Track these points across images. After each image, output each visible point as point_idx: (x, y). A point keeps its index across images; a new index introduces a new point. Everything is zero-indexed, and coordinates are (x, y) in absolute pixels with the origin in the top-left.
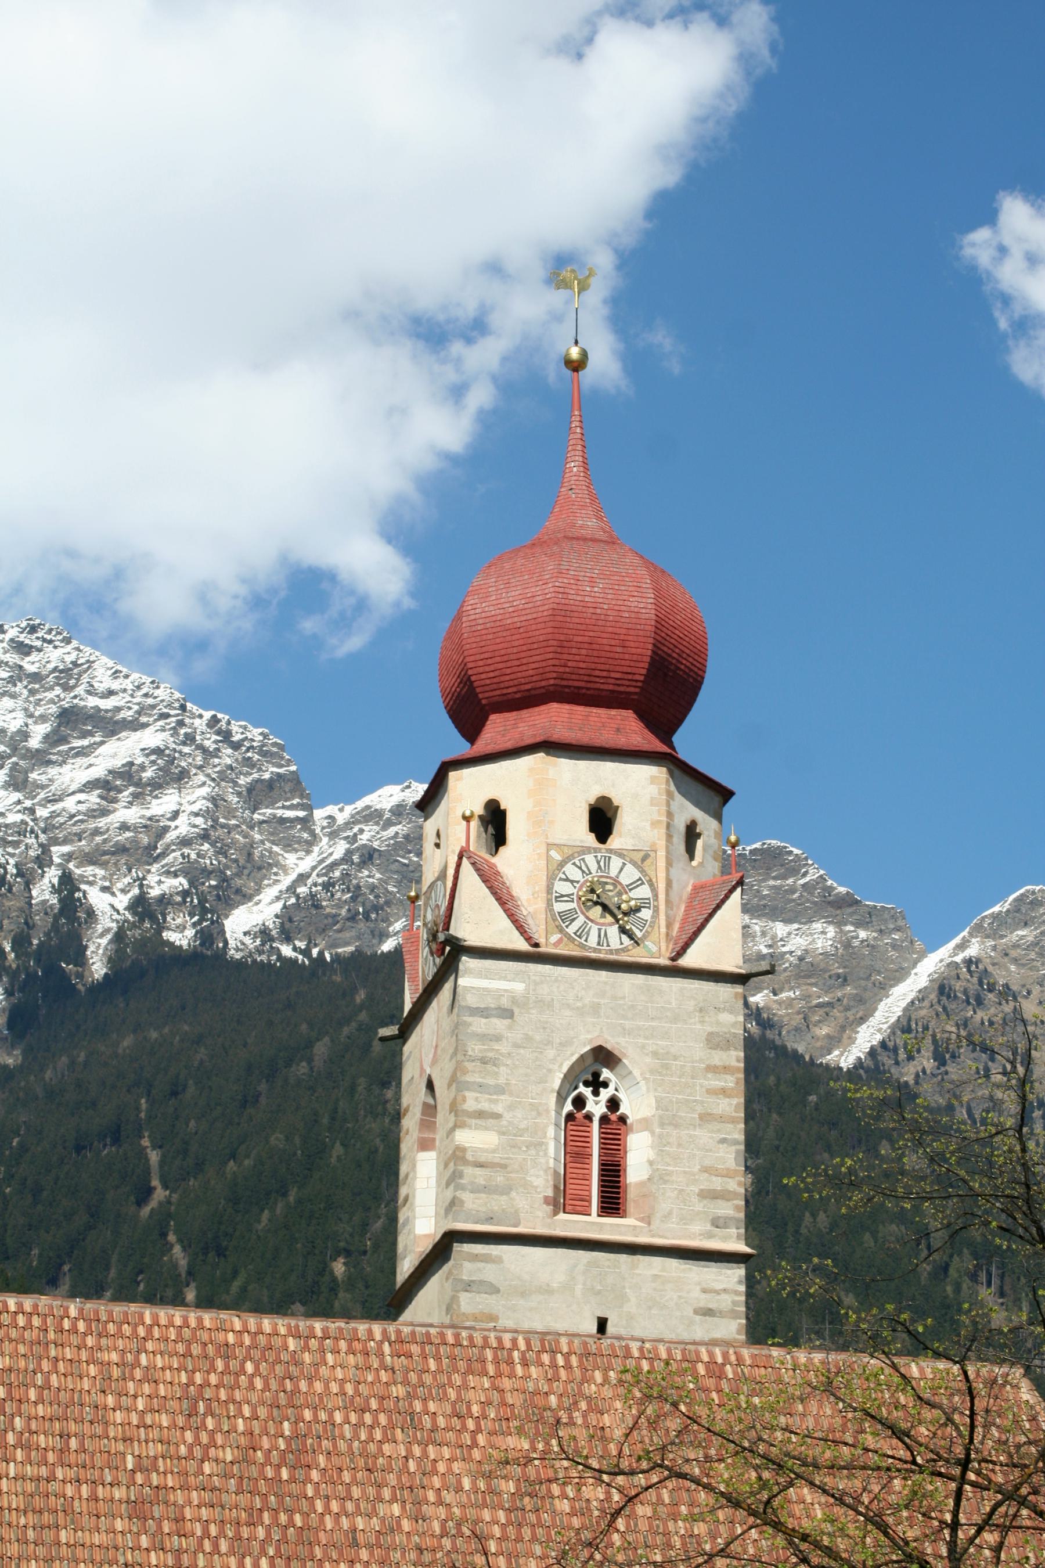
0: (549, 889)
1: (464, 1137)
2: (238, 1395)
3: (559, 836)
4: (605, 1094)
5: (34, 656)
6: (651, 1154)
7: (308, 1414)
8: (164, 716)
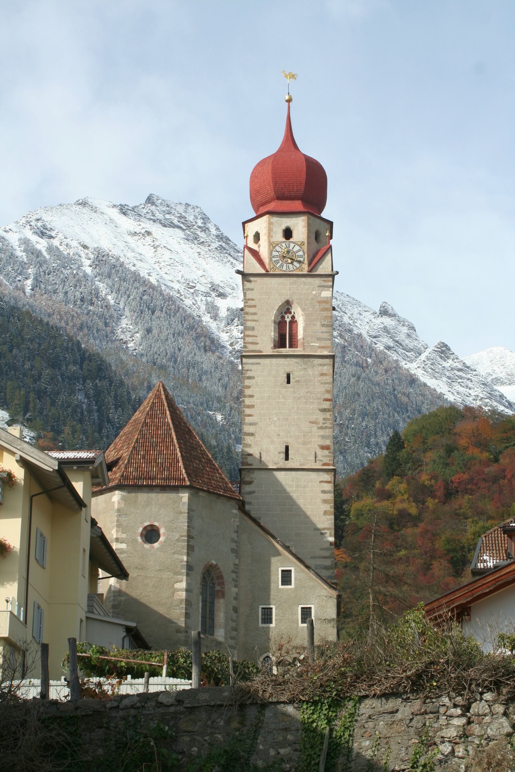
0: (271, 253)
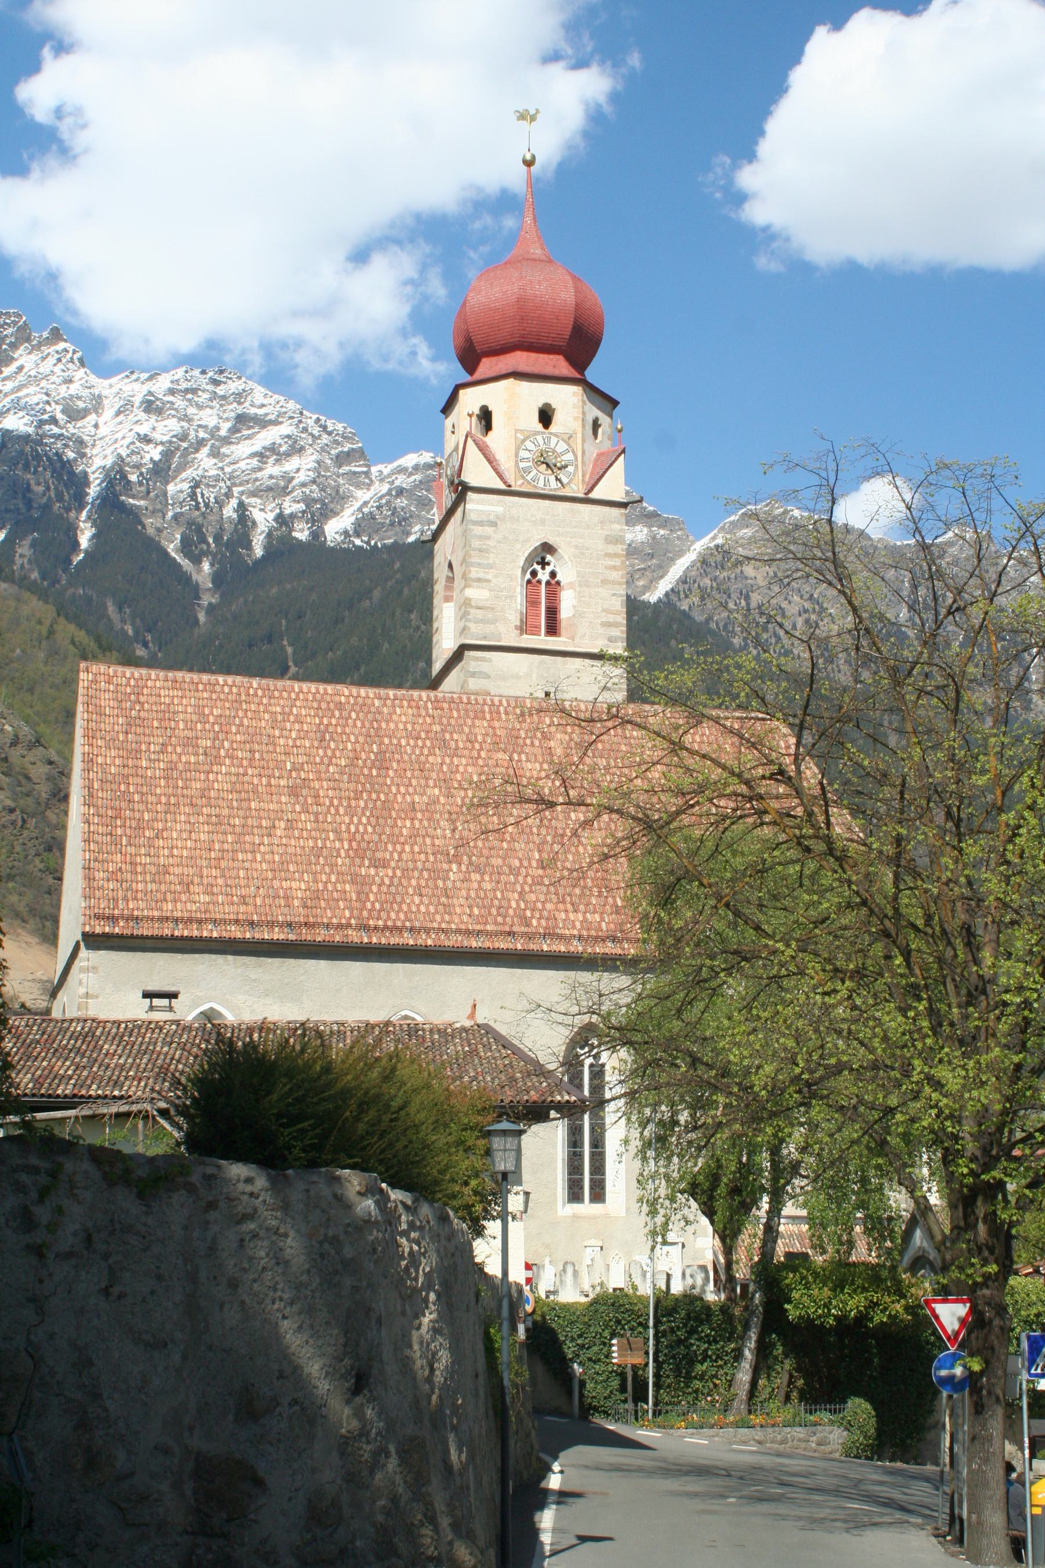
0: (517, 455)
1: (469, 592)
2: (347, 730)
3: (523, 426)
4: (548, 569)
5: (222, 387)
6: (575, 602)
7: (386, 741)
8: (291, 418)
